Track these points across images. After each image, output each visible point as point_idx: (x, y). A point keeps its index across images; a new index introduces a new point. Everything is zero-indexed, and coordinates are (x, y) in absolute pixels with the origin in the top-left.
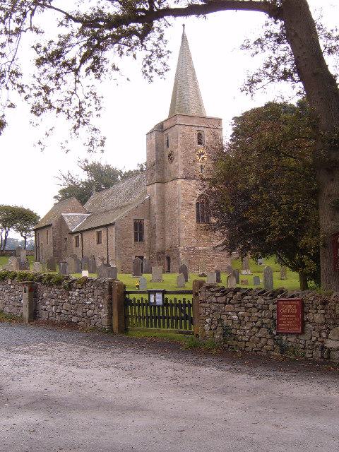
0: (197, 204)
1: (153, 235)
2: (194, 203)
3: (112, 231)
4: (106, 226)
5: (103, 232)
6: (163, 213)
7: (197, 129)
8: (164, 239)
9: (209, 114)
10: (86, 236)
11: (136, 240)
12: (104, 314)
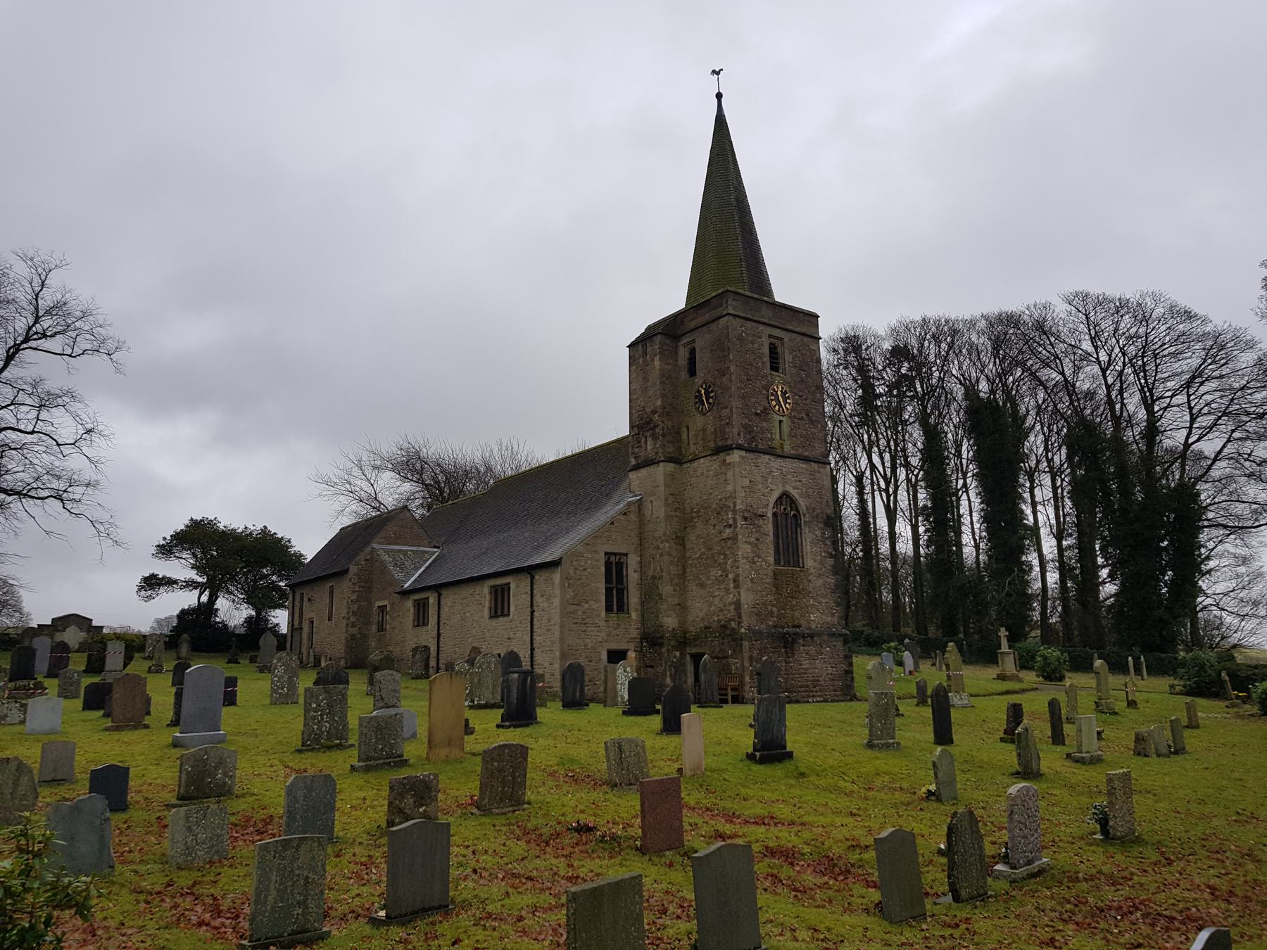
0: (775, 514)
1: (650, 594)
2: (770, 515)
4: (531, 570)
5: (518, 589)
6: (680, 541)
8: (682, 607)
10: (451, 599)
11: (609, 609)
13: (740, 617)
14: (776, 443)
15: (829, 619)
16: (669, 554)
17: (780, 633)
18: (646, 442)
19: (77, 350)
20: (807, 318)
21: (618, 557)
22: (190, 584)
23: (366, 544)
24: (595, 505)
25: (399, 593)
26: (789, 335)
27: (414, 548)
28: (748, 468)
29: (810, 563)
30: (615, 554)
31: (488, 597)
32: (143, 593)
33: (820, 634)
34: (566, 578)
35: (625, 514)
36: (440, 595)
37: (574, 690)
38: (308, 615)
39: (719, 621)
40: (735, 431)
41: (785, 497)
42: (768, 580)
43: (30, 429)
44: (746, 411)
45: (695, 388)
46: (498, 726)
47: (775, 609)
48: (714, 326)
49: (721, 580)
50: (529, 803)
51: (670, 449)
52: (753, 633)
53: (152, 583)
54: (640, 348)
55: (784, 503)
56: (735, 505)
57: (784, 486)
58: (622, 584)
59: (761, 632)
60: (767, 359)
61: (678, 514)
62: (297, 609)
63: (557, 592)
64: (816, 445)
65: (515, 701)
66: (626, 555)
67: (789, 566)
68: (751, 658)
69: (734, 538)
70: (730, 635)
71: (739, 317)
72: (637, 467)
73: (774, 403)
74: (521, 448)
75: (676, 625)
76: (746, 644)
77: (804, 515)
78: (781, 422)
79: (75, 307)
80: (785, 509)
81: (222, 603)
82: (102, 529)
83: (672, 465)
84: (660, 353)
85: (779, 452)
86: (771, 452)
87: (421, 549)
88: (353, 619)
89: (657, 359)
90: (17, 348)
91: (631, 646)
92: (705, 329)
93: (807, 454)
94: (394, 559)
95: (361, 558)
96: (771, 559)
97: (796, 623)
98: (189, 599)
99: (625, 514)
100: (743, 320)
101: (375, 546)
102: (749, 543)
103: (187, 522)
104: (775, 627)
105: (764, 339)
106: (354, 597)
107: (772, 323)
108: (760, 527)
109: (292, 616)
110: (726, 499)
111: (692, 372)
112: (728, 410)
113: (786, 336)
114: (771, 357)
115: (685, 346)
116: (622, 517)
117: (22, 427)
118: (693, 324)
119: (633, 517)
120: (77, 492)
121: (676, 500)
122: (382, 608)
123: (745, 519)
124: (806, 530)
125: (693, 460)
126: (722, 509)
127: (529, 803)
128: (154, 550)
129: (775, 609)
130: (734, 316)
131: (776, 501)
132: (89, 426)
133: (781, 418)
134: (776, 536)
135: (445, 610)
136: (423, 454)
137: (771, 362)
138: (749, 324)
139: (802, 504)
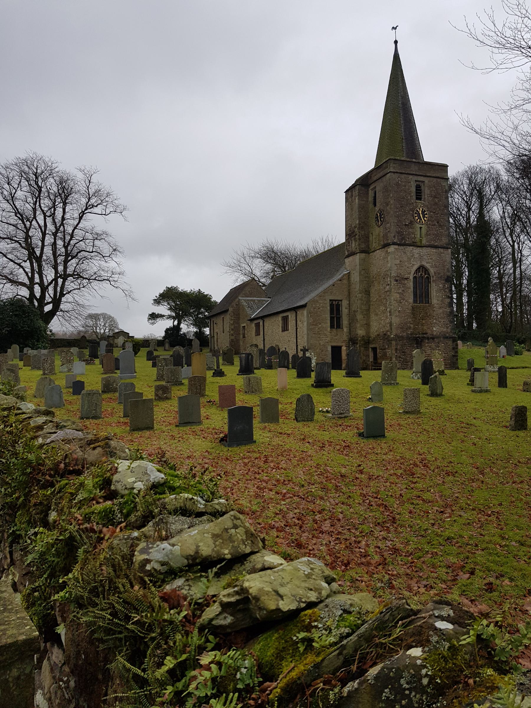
0: (415, 278)
2: (411, 278)
3: (303, 314)
4: (295, 309)
5: (291, 316)
6: (367, 292)
7: (416, 178)
9: (426, 160)
10: (268, 322)
11: (332, 326)
12: (384, 389)
13: (391, 330)
14: (417, 240)
15: (445, 330)
16: (361, 300)
17: (414, 337)
18: (352, 243)
19: (108, 212)
20: (441, 168)
21: (337, 302)
22: (170, 317)
23: (237, 297)
24: (332, 276)
25: (249, 320)
26: (429, 178)
27: (259, 299)
28: (399, 254)
29: (435, 301)
30: (335, 300)
31: (281, 322)
32: (150, 321)
33: (438, 337)
34: (309, 313)
35: (341, 280)
36: (264, 321)
37: (284, 362)
38: (216, 331)
39: (383, 332)
40: (393, 235)
41: (422, 268)
42: (408, 311)
43: (91, 251)
44: (399, 224)
45: (376, 213)
46: (238, 375)
47: (412, 326)
48: (384, 179)
49: (384, 312)
50: (207, 396)
51: (363, 246)
52: (398, 337)
53: (153, 317)
54: (350, 193)
55: (421, 271)
56: (391, 273)
57: (421, 262)
58: (339, 314)
59: (402, 337)
60: (414, 194)
61: (367, 279)
62: (212, 328)
63: (306, 319)
64: (443, 238)
65: (244, 365)
66: (341, 301)
67: (423, 303)
68: (396, 349)
69: (390, 291)
70: (386, 339)
71: (397, 172)
72: (348, 256)
73: (417, 218)
74: (334, 240)
75: (365, 334)
76: (394, 343)
77: (433, 277)
78: (421, 228)
79: (104, 191)
80: (421, 274)
81: (182, 326)
82: (127, 293)
83: (364, 254)
84: (359, 195)
85: (419, 244)
86: (414, 244)
87: (262, 299)
88: (232, 332)
89: (357, 198)
90: (83, 213)
91: (344, 344)
92: (380, 180)
93: (436, 244)
94: (248, 304)
95: (234, 304)
96: (411, 300)
97: (424, 332)
98: (169, 323)
99: (341, 280)
100: (399, 174)
101: (240, 298)
102: (398, 293)
103: (165, 289)
104: (411, 334)
105: (412, 183)
106: (232, 322)
107: (417, 173)
108: (405, 284)
109: (210, 330)
110: (387, 271)
111: (375, 205)
112: (389, 224)
113: (426, 180)
114: (416, 193)
115: (372, 190)
116: (339, 282)
117: (88, 250)
118: (375, 178)
119: (345, 282)
120: (116, 277)
121: (365, 272)
122: (244, 327)
123: (397, 281)
124: (433, 285)
125: (374, 251)
126: (386, 276)
127: (207, 396)
128: (152, 302)
129: (412, 326)
130: (394, 172)
131: (416, 270)
132: (115, 248)
133: (421, 226)
134: (415, 288)
135: (266, 327)
136: (275, 248)
137: (416, 195)
138: (403, 176)
139: (432, 271)
